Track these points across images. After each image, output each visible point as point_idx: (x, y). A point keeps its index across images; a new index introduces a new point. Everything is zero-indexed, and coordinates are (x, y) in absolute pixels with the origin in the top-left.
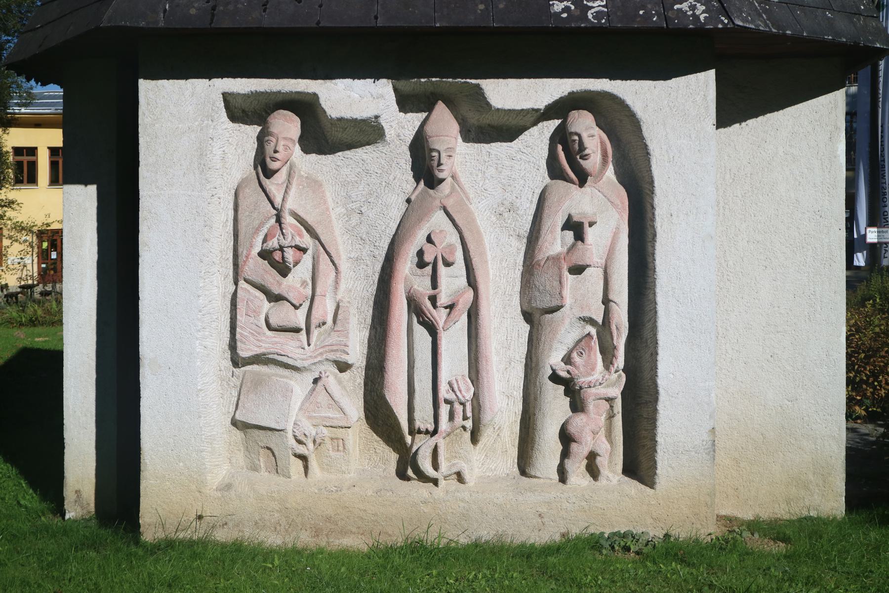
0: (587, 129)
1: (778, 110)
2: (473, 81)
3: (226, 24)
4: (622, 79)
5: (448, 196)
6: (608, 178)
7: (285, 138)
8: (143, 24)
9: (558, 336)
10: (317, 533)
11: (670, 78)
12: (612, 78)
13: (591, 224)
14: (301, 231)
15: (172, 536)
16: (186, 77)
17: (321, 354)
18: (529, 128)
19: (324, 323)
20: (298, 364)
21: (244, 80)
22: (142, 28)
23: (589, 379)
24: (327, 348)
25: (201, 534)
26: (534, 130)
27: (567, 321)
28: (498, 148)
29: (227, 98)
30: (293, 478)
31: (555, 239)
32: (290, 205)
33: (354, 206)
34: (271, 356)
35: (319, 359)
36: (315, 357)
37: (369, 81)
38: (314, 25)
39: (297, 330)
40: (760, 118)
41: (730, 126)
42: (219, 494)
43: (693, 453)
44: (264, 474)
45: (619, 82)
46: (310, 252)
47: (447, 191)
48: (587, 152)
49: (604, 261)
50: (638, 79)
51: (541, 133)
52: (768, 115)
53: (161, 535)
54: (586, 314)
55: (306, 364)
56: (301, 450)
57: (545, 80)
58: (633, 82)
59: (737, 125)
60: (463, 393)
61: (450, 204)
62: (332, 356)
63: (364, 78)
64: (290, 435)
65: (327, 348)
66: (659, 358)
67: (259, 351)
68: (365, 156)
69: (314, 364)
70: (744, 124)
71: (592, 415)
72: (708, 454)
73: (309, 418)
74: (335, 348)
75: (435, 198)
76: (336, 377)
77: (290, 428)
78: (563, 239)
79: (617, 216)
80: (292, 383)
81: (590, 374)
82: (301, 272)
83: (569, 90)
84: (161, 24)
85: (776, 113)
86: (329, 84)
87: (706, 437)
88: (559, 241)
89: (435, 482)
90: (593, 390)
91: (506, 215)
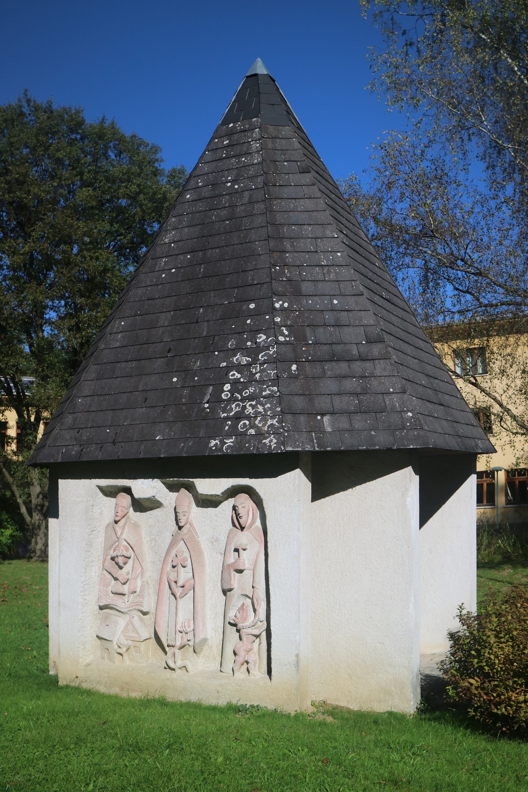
0: (241, 504)
1: (373, 480)
2: (191, 480)
3: (85, 459)
4: (255, 478)
5: (186, 534)
6: (257, 527)
7: (121, 506)
8: (52, 461)
9: (232, 603)
10: (122, 689)
11: (277, 476)
12: (251, 478)
13: (244, 550)
14: (128, 548)
15: (69, 684)
16: (80, 479)
17: (132, 606)
18: (222, 502)
19: (135, 592)
20: (122, 610)
21: (104, 480)
22: (51, 463)
23: (243, 624)
24: (134, 604)
25: (77, 685)
26: (226, 503)
27: (236, 596)
28: (210, 511)
29: (101, 488)
30: (116, 663)
31: (230, 556)
32: (124, 536)
33: (153, 537)
34: (112, 606)
35: (131, 608)
36: (130, 607)
37: (151, 480)
38: (117, 458)
39: (124, 595)
40: (363, 485)
41: (347, 490)
42: (84, 668)
43: (288, 666)
44: (106, 661)
45: (253, 480)
46: (132, 558)
47: (185, 532)
48: (240, 515)
49: (253, 567)
50: (262, 478)
51: (229, 504)
52: (368, 483)
53: (65, 683)
54: (244, 593)
55: (126, 610)
56: (120, 651)
57: (221, 479)
58: (260, 479)
59: (350, 490)
60: (186, 628)
61: (186, 537)
62: (137, 607)
63: (148, 478)
64: (115, 643)
65: (134, 604)
66: (271, 616)
67: (106, 603)
68: (157, 514)
69: (129, 611)
70: (354, 489)
71: (245, 642)
72: (295, 667)
73: (125, 636)
74: (138, 604)
75: (180, 535)
76: (140, 617)
77: (115, 641)
78: (234, 555)
79: (258, 545)
80: (120, 619)
81: (243, 622)
82: (127, 568)
83: (231, 485)
84: (60, 460)
85: (372, 482)
86: (140, 481)
87: (294, 658)
88: (232, 557)
89: (174, 670)
90: (245, 630)
91: (215, 543)
